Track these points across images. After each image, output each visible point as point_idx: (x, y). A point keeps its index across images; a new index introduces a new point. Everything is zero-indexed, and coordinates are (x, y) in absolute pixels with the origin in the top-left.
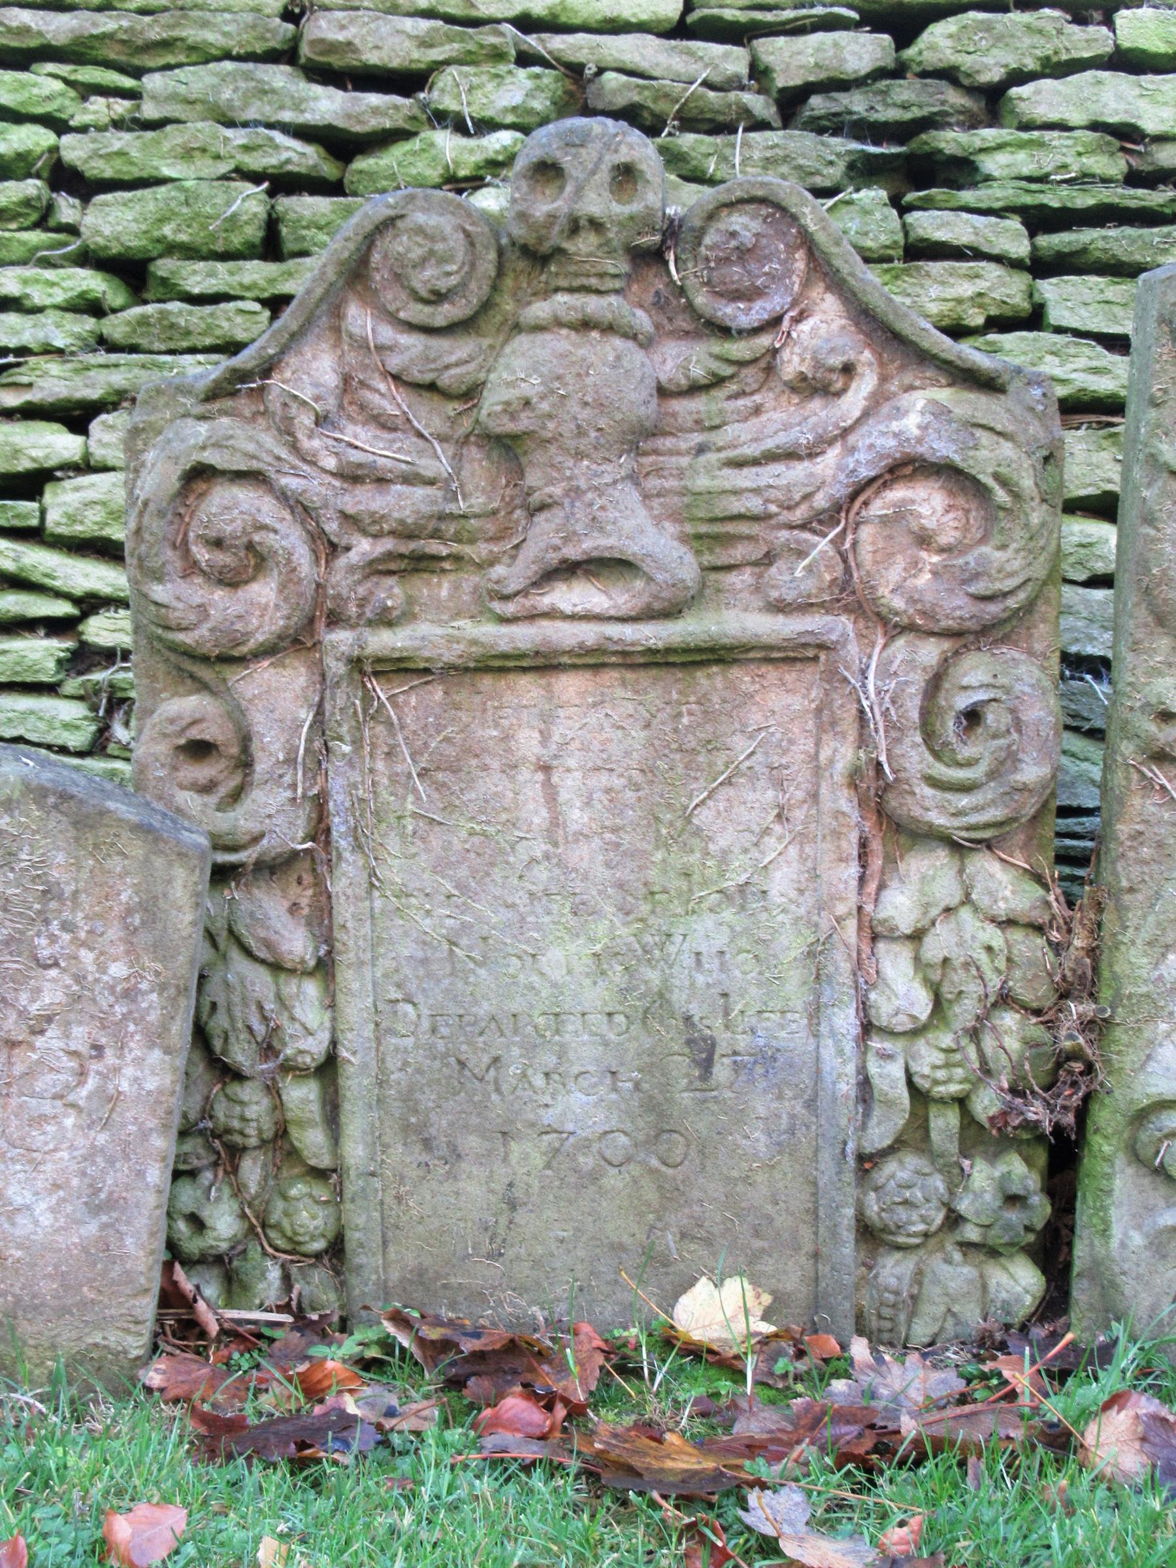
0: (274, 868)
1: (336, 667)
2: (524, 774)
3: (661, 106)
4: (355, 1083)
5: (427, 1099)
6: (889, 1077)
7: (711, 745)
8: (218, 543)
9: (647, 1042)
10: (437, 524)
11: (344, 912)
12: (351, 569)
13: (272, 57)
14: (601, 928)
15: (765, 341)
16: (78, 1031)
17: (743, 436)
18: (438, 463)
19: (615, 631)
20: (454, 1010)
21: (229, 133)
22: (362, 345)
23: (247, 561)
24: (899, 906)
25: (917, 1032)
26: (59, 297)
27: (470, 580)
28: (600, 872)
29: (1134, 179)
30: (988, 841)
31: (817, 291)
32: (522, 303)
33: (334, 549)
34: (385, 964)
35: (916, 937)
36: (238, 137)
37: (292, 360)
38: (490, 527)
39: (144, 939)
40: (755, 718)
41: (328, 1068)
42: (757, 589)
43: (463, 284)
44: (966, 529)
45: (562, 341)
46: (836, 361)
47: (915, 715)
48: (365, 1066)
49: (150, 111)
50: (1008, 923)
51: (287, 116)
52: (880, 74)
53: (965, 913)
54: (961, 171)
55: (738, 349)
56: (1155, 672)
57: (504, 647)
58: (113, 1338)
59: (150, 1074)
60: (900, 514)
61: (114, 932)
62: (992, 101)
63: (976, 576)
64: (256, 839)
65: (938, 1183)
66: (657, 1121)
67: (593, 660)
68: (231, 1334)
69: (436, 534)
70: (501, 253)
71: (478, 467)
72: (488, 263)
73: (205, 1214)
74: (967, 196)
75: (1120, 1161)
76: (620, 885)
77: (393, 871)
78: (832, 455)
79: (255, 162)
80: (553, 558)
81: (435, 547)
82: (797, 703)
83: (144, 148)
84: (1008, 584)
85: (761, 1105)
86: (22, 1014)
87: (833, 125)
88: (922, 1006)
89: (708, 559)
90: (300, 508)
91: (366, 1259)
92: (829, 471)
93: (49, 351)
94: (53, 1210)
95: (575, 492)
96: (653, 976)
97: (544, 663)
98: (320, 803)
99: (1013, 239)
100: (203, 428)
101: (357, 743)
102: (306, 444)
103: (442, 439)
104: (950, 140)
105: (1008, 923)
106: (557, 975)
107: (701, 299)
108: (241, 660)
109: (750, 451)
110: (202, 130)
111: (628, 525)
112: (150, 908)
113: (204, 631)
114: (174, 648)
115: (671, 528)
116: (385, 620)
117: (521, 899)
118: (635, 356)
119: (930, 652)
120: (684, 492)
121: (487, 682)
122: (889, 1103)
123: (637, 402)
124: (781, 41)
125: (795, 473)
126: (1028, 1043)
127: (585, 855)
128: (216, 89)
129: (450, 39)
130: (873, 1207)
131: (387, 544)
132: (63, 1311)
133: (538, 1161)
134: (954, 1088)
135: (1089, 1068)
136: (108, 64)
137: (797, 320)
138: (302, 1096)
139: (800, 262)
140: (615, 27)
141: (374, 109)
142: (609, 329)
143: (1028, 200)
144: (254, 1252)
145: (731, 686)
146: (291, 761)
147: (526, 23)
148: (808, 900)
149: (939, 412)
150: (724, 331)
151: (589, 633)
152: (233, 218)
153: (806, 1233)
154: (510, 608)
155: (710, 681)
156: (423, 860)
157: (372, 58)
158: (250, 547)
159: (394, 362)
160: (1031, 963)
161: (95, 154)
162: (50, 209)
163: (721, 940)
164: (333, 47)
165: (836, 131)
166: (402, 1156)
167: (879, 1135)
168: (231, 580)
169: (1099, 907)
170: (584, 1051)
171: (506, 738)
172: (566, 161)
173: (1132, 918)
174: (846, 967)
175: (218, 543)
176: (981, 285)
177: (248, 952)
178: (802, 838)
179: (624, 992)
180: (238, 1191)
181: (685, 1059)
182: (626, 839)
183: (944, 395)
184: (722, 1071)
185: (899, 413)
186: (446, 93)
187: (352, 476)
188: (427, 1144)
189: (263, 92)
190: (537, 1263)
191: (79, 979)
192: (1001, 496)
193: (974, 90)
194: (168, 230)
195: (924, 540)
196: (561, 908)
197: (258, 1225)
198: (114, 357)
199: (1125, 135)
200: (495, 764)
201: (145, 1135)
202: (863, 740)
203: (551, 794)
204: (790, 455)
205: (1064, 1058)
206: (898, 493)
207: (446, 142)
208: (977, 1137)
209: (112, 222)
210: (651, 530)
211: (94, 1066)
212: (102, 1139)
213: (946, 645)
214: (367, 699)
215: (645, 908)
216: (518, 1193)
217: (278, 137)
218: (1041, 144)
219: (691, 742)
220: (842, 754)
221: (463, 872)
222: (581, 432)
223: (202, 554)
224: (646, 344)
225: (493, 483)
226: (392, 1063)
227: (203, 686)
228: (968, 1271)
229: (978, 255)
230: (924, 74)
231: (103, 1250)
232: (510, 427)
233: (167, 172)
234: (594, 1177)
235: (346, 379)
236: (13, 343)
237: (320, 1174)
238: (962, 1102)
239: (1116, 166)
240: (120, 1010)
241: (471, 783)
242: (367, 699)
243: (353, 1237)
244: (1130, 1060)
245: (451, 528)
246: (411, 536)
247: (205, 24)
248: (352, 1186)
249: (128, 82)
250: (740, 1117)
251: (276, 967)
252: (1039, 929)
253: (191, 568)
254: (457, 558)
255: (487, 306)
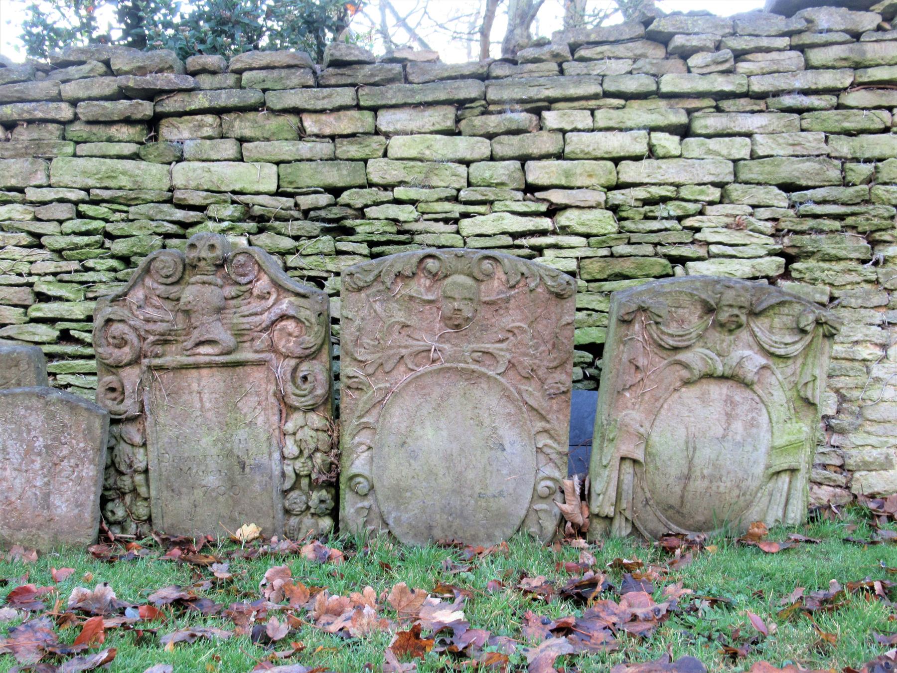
0: (132, 419)
1: (145, 368)
2: (194, 394)
3: (270, 215)
4: (152, 474)
5: (173, 479)
6: (289, 470)
7: (241, 386)
8: (114, 338)
9: (228, 463)
10: (170, 332)
11: (148, 431)
12: (148, 344)
13: (165, 202)
14: (215, 434)
15: (249, 286)
16: (72, 461)
17: (245, 310)
18: (171, 317)
19: (213, 358)
20: (178, 455)
21: (151, 223)
22: (149, 288)
23: (122, 343)
24: (290, 426)
25: (296, 458)
26: (105, 267)
27: (180, 346)
28: (215, 419)
29: (399, 232)
30: (313, 409)
31: (262, 274)
32: (190, 277)
33: (145, 339)
34: (160, 444)
35: (294, 434)
36: (154, 224)
37: (132, 292)
38: (184, 333)
39: (88, 437)
40: (251, 379)
41: (146, 471)
42: (251, 347)
43: (174, 273)
44: (301, 331)
45: (198, 287)
46: (265, 291)
47: (289, 378)
48: (155, 471)
49: (131, 217)
50: (317, 430)
51: (168, 218)
52: (329, 205)
53: (306, 428)
54: (351, 231)
55: (243, 288)
56: (346, 366)
57: (186, 362)
58: (82, 540)
59: (90, 471)
60: (282, 329)
61: (81, 435)
62: (361, 213)
63: (302, 343)
64: (125, 412)
65: (304, 498)
66: (231, 483)
67: (210, 365)
68: (119, 540)
69: (169, 335)
70: (184, 266)
71: (180, 316)
72: (181, 268)
73: (115, 510)
74: (352, 238)
75: (347, 490)
76: (219, 422)
77: (162, 420)
78: (266, 313)
79: (159, 230)
80: (198, 340)
81: (169, 338)
82: (262, 375)
83: (129, 227)
84: (311, 345)
85: (258, 478)
86: (58, 456)
87: (313, 220)
88: (296, 452)
89: (239, 340)
90: (135, 329)
91: (158, 522)
92: (266, 318)
93: (101, 282)
94: (67, 507)
95: (203, 324)
96: (229, 445)
97: (197, 367)
98: (142, 402)
99: (364, 249)
100: (110, 309)
101: (151, 387)
102: (135, 313)
103: (172, 311)
104: (348, 223)
105: (317, 430)
106: (204, 446)
107: (233, 276)
108: (121, 367)
109: (246, 313)
110: (144, 222)
111: (216, 332)
112: (90, 429)
113: (111, 360)
114: (104, 364)
115: (229, 332)
116: (157, 356)
117: (194, 426)
118: (217, 290)
119: (293, 362)
120: (231, 323)
121: (184, 371)
122: (290, 477)
123: (217, 302)
124: (302, 197)
125: (257, 319)
126: (323, 461)
127: (210, 415)
128: (148, 211)
129: (212, 197)
130: (287, 504)
131: (157, 337)
132: (69, 533)
133: (202, 494)
134: (305, 473)
135: (337, 467)
136: (120, 204)
137: (258, 281)
138: (139, 478)
139: (256, 267)
140: (258, 193)
141: (192, 216)
142: (210, 284)
143: (368, 239)
144: (129, 520)
145: (245, 371)
146: (133, 392)
147: (234, 192)
148: (267, 426)
149: (291, 303)
150: (240, 284)
151: (207, 359)
152: (152, 246)
153: (271, 511)
154: (189, 353)
155: (240, 370)
156: (169, 417)
157: (191, 202)
158: (123, 338)
159: (158, 292)
160: (323, 440)
161: (115, 229)
162: (103, 243)
163: (246, 436)
164: (180, 200)
165: (317, 221)
166: (166, 494)
167: (287, 485)
168: (118, 347)
169: (339, 425)
170: (212, 465)
171: (189, 385)
172: (197, 244)
173: (346, 428)
174: (275, 442)
175: (114, 338)
176: (355, 262)
177: (125, 441)
178: (265, 409)
179: (222, 449)
180: (125, 505)
181: (238, 467)
182: (221, 411)
183: (293, 299)
184: (247, 470)
185: (282, 304)
186: (212, 211)
187: (147, 321)
188: (173, 490)
189: (161, 212)
190: (202, 521)
191: (72, 447)
192: (307, 324)
193: (356, 209)
194: (134, 249)
195: (290, 335)
196: (204, 428)
197: (129, 513)
198: (119, 283)
199: (396, 221)
200: (187, 392)
201: (89, 487)
202: (277, 385)
203: (201, 400)
204: (256, 314)
205: (332, 463)
206: (283, 323)
207: (211, 224)
208: (314, 486)
209: (119, 247)
210: (223, 333)
211: (76, 470)
212: (79, 488)
213: (297, 360)
214: (153, 376)
215: (226, 428)
216: (196, 503)
217: (165, 223)
218: (372, 224)
219: (236, 385)
220: (272, 388)
221: (180, 420)
222: (203, 309)
223: (111, 340)
224: (221, 287)
225: (184, 322)
226: (163, 469)
227: (113, 374)
228: (313, 521)
229: (354, 253)
230: (341, 205)
231: (80, 516)
232: (186, 308)
233: (134, 233)
234: (216, 498)
235: (146, 297)
236: (91, 280)
237: (146, 499)
238: (309, 476)
239: (394, 229)
240: (82, 455)
241: (180, 397)
242: (153, 376)
243: (153, 515)
244: (348, 464)
245: (173, 333)
246: (163, 335)
247: (146, 193)
248: (153, 502)
249: (125, 208)
250: (253, 482)
251: (133, 445)
252: (325, 431)
253: (109, 344)
254: (176, 340)
255: (181, 278)
